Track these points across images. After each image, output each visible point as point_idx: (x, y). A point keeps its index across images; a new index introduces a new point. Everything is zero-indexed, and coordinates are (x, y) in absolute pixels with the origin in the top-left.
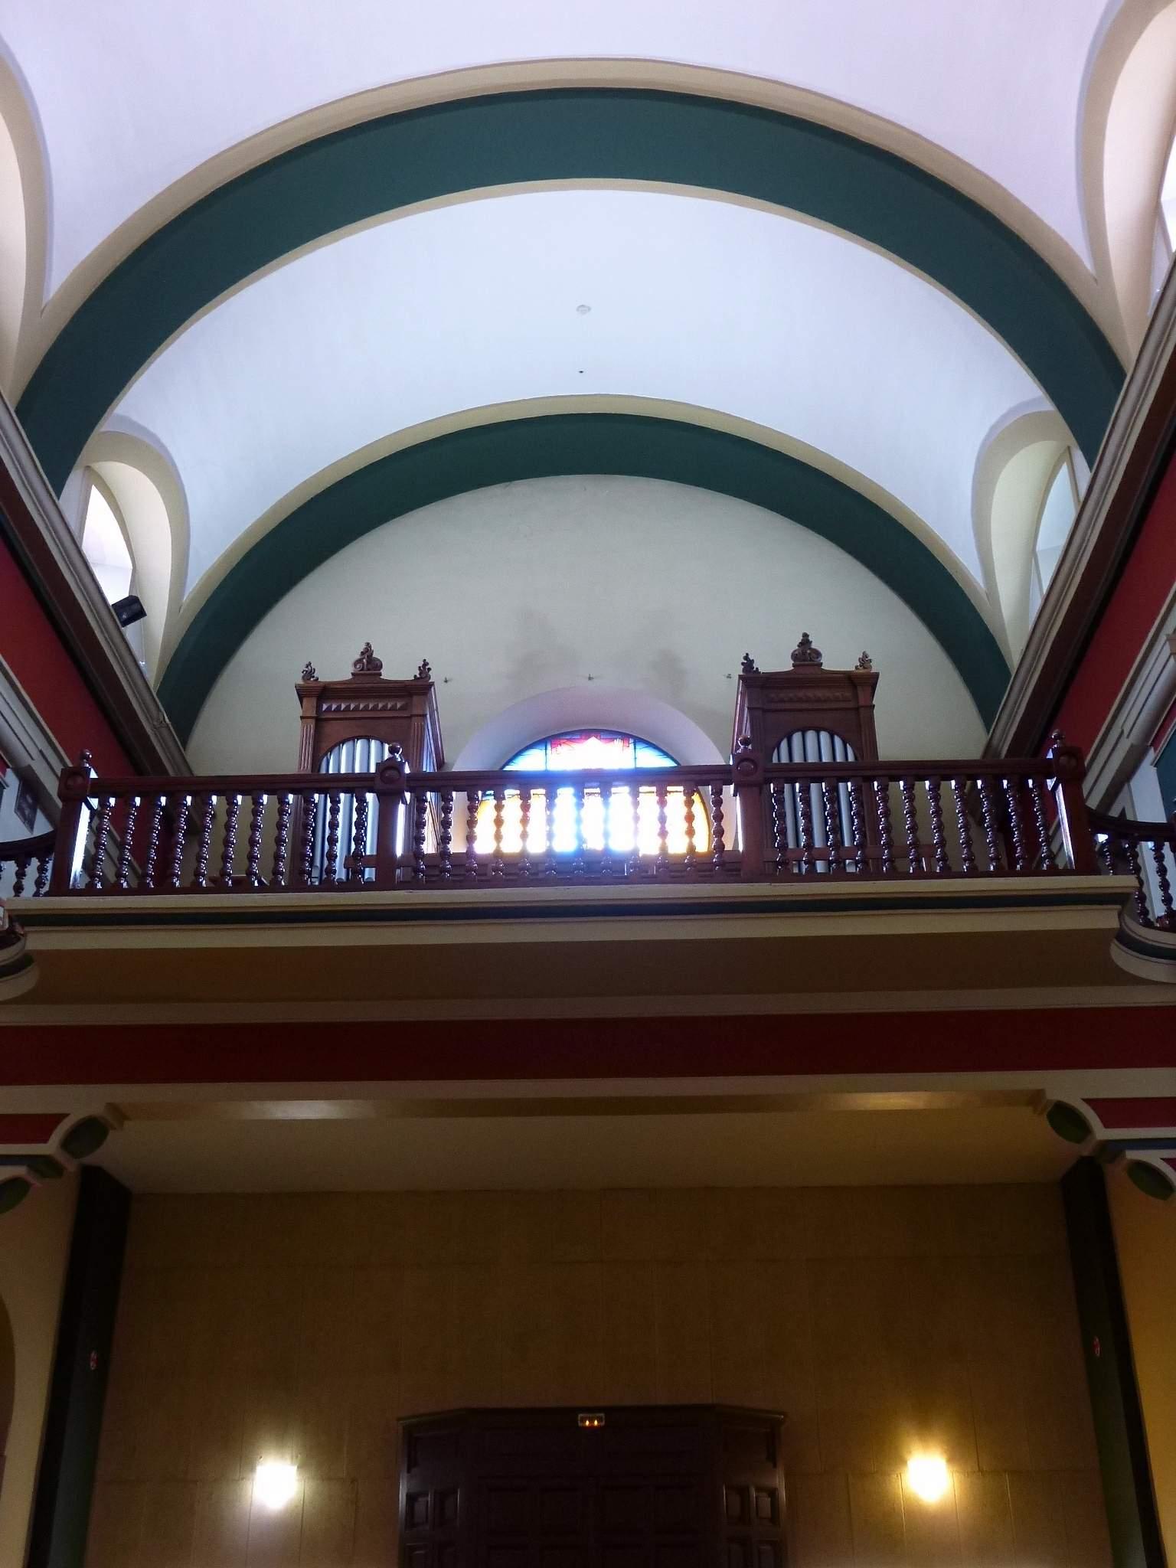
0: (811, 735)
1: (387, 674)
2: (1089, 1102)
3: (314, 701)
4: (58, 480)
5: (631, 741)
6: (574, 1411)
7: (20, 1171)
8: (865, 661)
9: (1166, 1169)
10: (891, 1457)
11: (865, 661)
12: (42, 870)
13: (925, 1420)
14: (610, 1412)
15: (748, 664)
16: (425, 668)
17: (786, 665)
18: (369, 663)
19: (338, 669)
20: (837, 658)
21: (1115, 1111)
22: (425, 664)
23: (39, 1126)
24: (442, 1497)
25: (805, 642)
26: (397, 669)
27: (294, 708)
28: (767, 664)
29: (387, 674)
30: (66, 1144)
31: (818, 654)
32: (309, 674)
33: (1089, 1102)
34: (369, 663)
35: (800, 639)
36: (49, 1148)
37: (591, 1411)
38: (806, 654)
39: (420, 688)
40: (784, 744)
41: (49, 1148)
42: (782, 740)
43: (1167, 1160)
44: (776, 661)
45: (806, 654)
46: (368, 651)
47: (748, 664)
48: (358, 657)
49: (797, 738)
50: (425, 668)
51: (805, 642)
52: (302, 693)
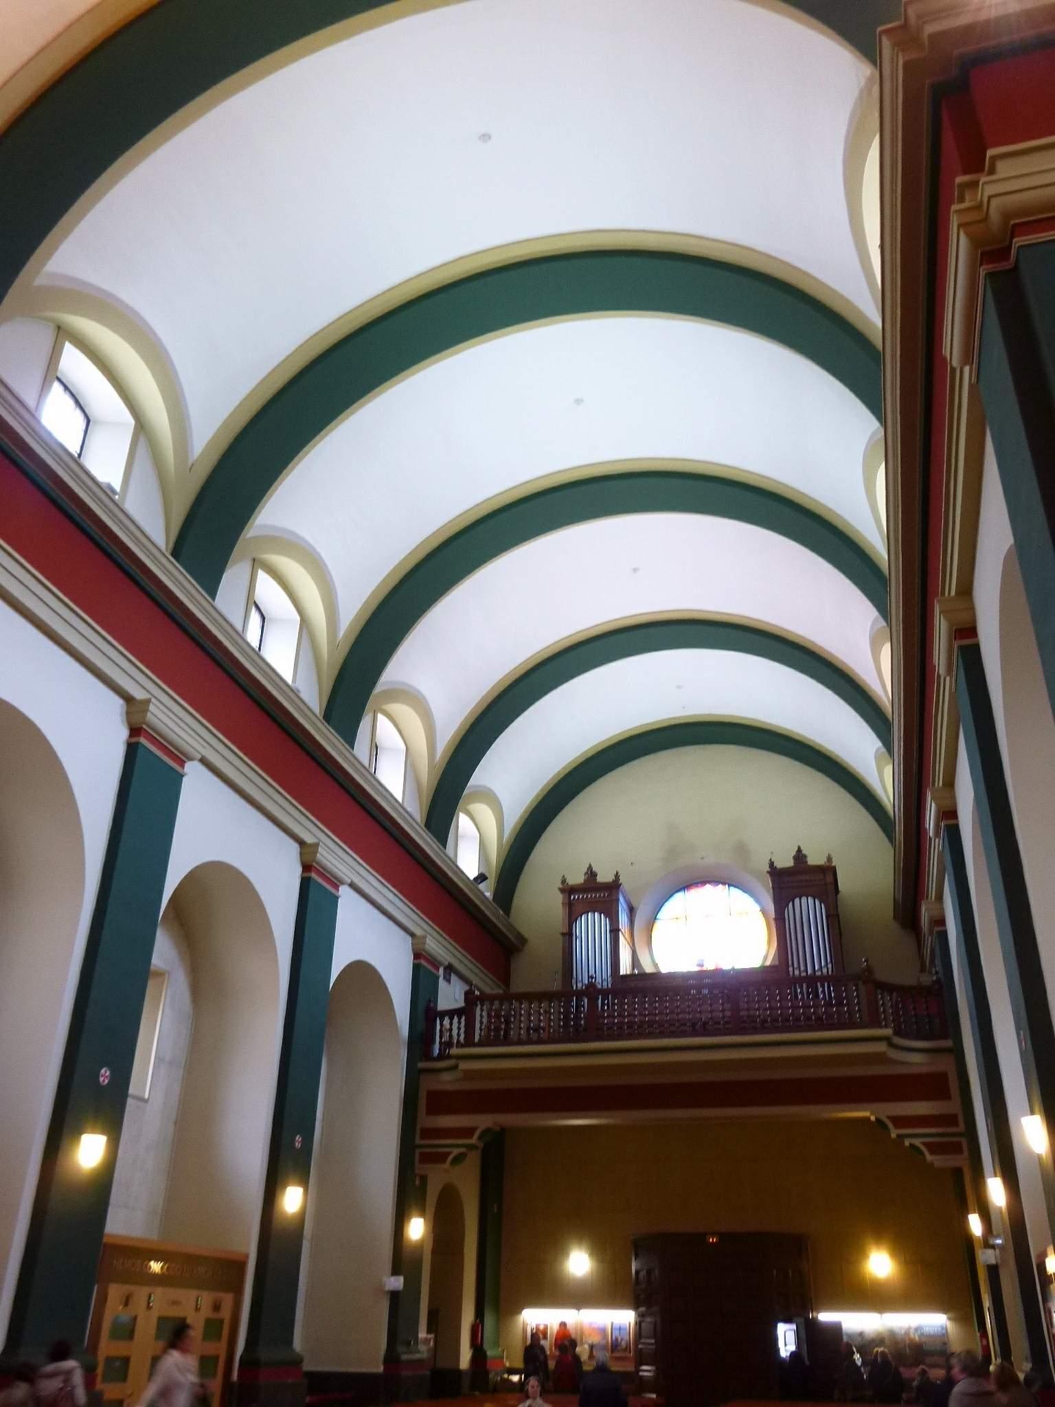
0: (804, 899)
1: (600, 879)
2: (888, 1117)
3: (567, 894)
4: (443, 842)
5: (727, 886)
6: (703, 1236)
7: (462, 1150)
8: (829, 859)
9: (923, 1148)
10: (861, 1254)
11: (829, 859)
12: (459, 1023)
13: (580, 1239)
14: (721, 1235)
15: (771, 864)
16: (617, 876)
17: (790, 863)
18: (591, 874)
19: (577, 878)
20: (815, 858)
21: (899, 1121)
22: (617, 873)
23: (468, 1132)
24: (649, 1272)
25: (799, 850)
26: (604, 877)
27: (560, 898)
28: (779, 864)
29: (600, 879)
30: (480, 1138)
31: (805, 856)
32: (564, 881)
33: (888, 1117)
34: (591, 874)
35: (588, 865)
36: (474, 1140)
37: (713, 1234)
38: (800, 856)
39: (614, 887)
40: (790, 905)
41: (474, 1140)
42: (789, 902)
43: (924, 1144)
44: (785, 861)
45: (800, 856)
46: (590, 868)
47: (771, 864)
48: (586, 870)
49: (797, 901)
50: (617, 876)
51: (799, 850)
52: (562, 891)
